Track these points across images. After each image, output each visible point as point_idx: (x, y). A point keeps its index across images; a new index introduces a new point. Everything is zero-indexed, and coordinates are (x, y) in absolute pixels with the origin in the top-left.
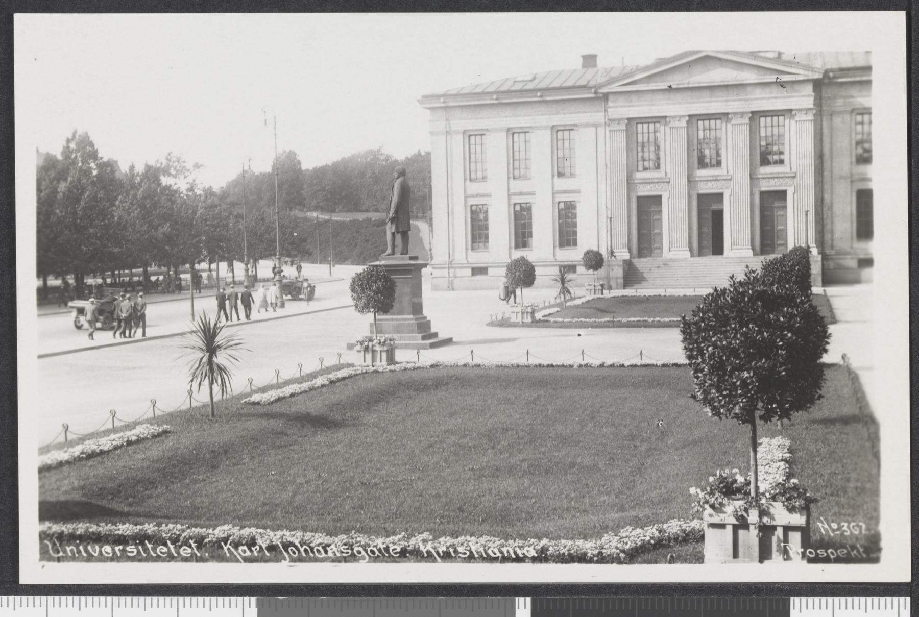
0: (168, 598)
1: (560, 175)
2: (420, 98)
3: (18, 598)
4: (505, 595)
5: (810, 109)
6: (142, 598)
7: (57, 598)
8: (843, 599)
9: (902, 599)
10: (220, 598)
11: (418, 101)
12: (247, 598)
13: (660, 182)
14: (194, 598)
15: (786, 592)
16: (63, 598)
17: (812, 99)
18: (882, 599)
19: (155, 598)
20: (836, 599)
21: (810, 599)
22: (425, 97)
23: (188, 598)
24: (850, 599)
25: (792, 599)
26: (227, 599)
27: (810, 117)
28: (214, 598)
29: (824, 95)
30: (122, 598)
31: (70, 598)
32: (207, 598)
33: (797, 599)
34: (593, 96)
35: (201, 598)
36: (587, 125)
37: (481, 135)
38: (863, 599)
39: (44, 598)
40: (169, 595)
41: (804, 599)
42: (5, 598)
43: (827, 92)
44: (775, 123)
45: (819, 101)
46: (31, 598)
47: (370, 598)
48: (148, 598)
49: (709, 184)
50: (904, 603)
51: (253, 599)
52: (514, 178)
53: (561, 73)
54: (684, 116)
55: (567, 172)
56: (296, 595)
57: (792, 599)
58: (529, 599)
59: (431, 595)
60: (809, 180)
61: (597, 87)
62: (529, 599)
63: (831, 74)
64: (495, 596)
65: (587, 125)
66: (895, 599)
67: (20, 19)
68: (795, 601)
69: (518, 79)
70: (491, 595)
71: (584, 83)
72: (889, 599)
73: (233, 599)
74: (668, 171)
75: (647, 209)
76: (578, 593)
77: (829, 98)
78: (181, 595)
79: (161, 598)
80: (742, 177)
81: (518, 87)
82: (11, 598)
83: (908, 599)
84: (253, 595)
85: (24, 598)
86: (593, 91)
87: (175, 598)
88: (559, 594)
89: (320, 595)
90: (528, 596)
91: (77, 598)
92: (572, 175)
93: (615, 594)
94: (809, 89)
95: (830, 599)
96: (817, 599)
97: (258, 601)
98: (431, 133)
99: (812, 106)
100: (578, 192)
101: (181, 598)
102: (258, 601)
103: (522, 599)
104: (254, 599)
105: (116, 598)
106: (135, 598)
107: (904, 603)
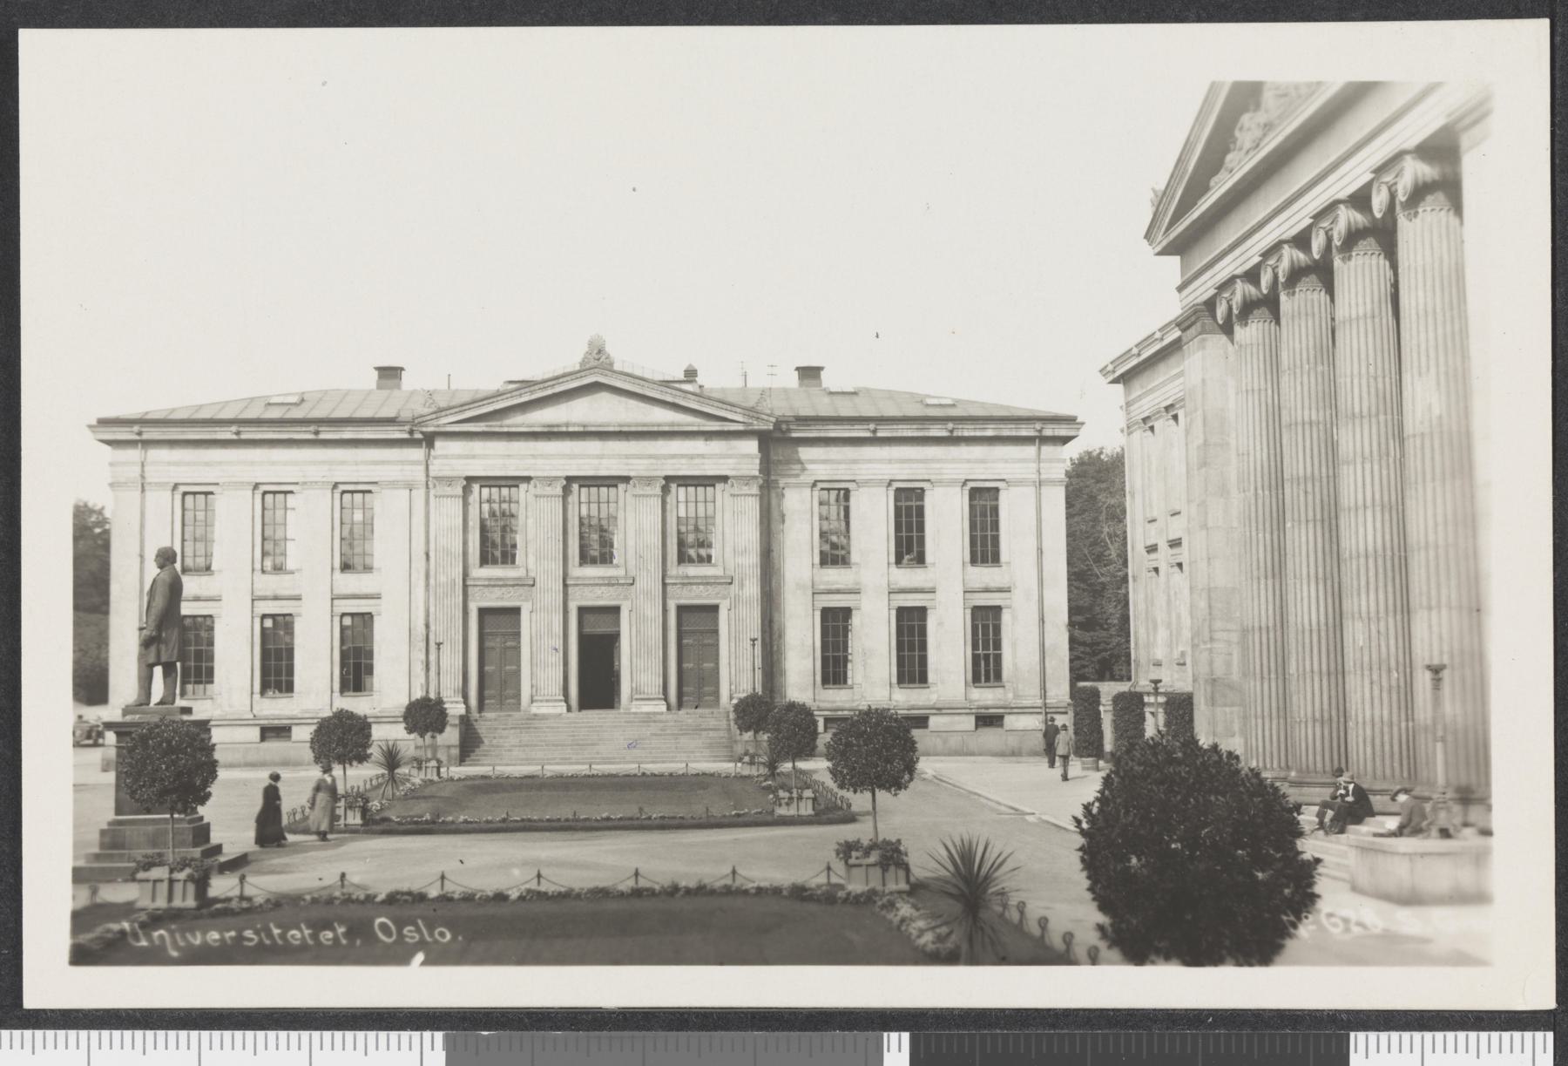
0: (294, 1034)
1: (346, 567)
2: (94, 422)
3: (39, 1033)
4: (866, 1029)
5: (754, 477)
6: (250, 1034)
7: (105, 1033)
8: (1439, 1035)
9: (1539, 1035)
10: (383, 1034)
11: (90, 427)
12: (427, 1034)
13: (518, 583)
14: (338, 1034)
15: (1336, 1027)
16: (117, 1033)
17: (758, 461)
18: (1506, 1035)
19: (272, 1034)
20: (1428, 1035)
21: (1384, 1035)
22: (104, 422)
23: (327, 1034)
24: (1450, 1035)
25: (1352, 1035)
26: (394, 1035)
27: (755, 490)
28: (372, 1034)
29: (774, 457)
30: (216, 1034)
31: (128, 1033)
32: (360, 1034)
33: (1361, 1035)
34: (406, 436)
35: (349, 1035)
36: (393, 484)
37: (206, 494)
38: (1473, 1035)
39: (83, 1033)
40: (295, 1029)
41: (1372, 1035)
42: (5, 1033)
43: (778, 453)
44: (701, 498)
45: (767, 466)
46: (61, 1033)
47: (636, 1033)
48: (261, 1034)
49: (598, 591)
50: (1544, 1041)
51: (439, 1035)
52: (263, 571)
53: (348, 393)
54: (557, 478)
55: (357, 561)
56: (511, 1029)
57: (1352, 1035)
58: (906, 1036)
59: (739, 1029)
60: (752, 589)
61: (414, 423)
62: (906, 1036)
63: (784, 427)
64: (850, 1030)
65: (393, 484)
66: (1528, 1035)
67: (1539, 30)
68: (1358, 1039)
69: (273, 400)
70: (842, 1029)
71: (392, 414)
72: (1517, 1035)
73: (405, 1035)
74: (531, 566)
75: (499, 624)
76: (990, 1026)
77: (780, 462)
78: (316, 1029)
79: (283, 1034)
80: (649, 581)
81: (275, 414)
82: (28, 1033)
83: (1550, 1035)
84: (438, 1029)
85: (50, 1033)
86: (407, 428)
87: (305, 1034)
88: (958, 1027)
89: (551, 1029)
90: (905, 1030)
91: (139, 1033)
92: (368, 569)
93: (1053, 1026)
94: (751, 446)
95: (1417, 1035)
96: (1395, 1035)
97: (446, 1040)
98: (111, 485)
99: (757, 473)
100: (377, 597)
101: (316, 1034)
102: (446, 1038)
103: (894, 1035)
104: (439, 1036)
105: (205, 1034)
106: (238, 1034)
107: (1544, 1041)
